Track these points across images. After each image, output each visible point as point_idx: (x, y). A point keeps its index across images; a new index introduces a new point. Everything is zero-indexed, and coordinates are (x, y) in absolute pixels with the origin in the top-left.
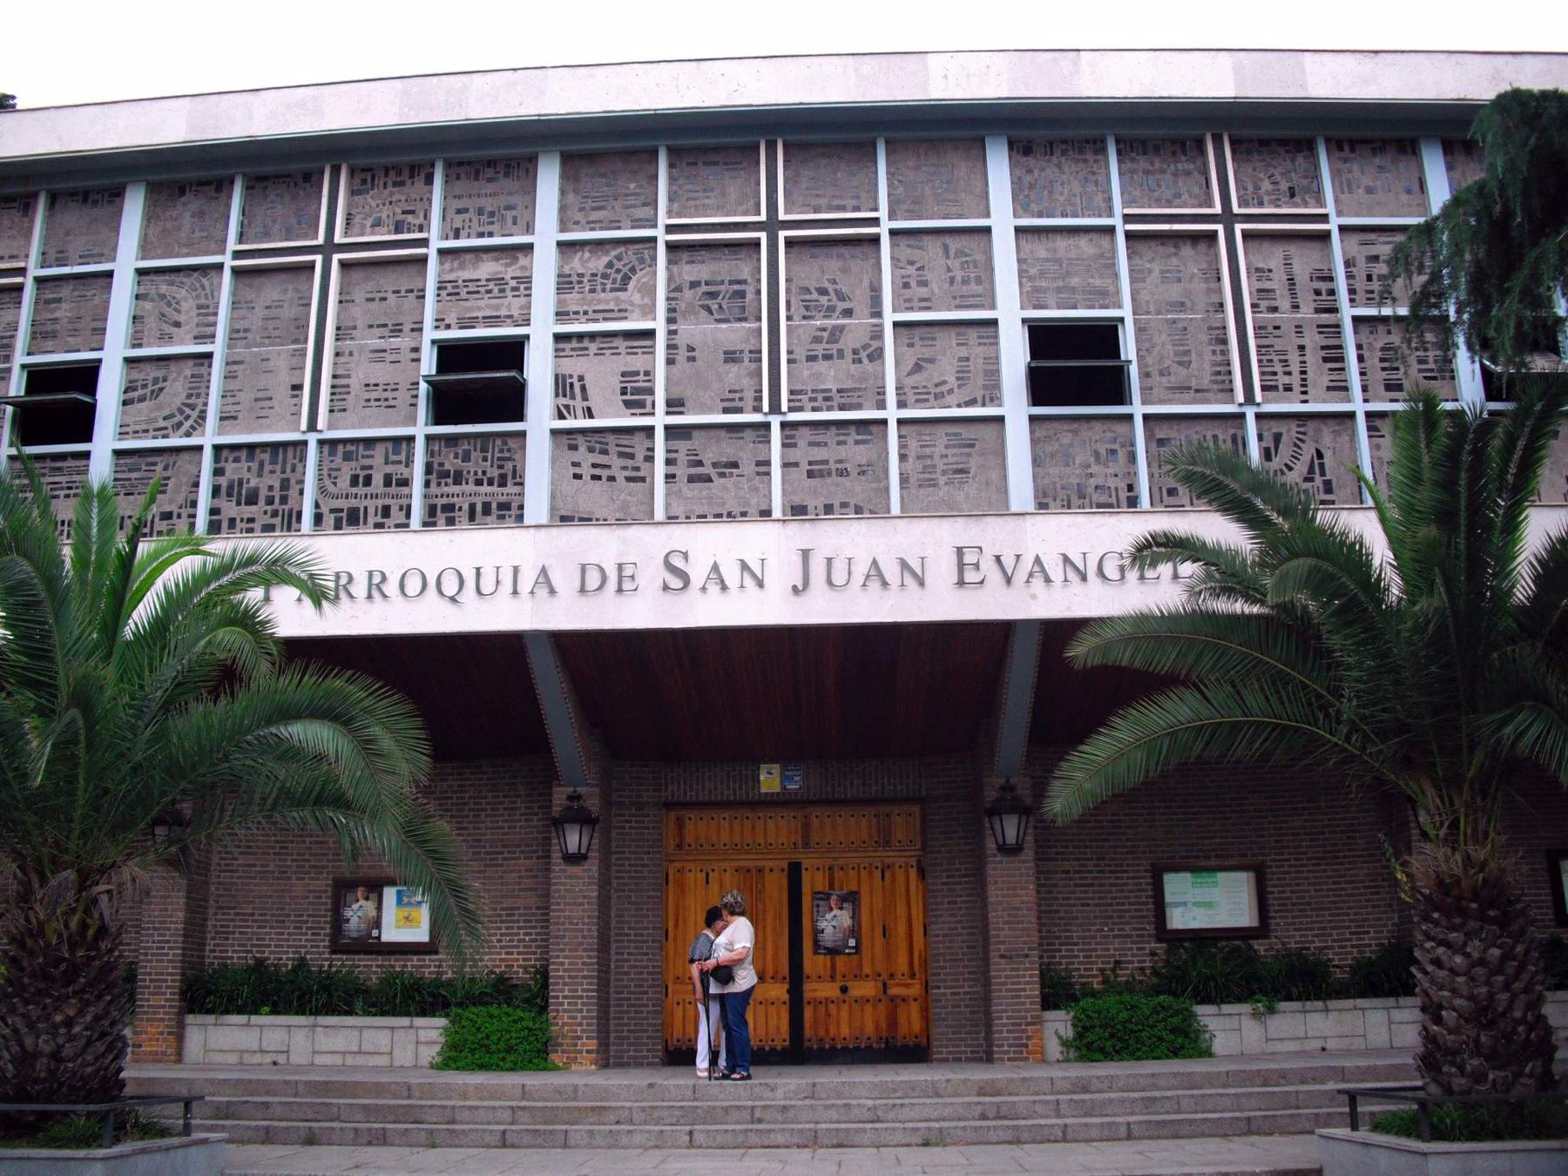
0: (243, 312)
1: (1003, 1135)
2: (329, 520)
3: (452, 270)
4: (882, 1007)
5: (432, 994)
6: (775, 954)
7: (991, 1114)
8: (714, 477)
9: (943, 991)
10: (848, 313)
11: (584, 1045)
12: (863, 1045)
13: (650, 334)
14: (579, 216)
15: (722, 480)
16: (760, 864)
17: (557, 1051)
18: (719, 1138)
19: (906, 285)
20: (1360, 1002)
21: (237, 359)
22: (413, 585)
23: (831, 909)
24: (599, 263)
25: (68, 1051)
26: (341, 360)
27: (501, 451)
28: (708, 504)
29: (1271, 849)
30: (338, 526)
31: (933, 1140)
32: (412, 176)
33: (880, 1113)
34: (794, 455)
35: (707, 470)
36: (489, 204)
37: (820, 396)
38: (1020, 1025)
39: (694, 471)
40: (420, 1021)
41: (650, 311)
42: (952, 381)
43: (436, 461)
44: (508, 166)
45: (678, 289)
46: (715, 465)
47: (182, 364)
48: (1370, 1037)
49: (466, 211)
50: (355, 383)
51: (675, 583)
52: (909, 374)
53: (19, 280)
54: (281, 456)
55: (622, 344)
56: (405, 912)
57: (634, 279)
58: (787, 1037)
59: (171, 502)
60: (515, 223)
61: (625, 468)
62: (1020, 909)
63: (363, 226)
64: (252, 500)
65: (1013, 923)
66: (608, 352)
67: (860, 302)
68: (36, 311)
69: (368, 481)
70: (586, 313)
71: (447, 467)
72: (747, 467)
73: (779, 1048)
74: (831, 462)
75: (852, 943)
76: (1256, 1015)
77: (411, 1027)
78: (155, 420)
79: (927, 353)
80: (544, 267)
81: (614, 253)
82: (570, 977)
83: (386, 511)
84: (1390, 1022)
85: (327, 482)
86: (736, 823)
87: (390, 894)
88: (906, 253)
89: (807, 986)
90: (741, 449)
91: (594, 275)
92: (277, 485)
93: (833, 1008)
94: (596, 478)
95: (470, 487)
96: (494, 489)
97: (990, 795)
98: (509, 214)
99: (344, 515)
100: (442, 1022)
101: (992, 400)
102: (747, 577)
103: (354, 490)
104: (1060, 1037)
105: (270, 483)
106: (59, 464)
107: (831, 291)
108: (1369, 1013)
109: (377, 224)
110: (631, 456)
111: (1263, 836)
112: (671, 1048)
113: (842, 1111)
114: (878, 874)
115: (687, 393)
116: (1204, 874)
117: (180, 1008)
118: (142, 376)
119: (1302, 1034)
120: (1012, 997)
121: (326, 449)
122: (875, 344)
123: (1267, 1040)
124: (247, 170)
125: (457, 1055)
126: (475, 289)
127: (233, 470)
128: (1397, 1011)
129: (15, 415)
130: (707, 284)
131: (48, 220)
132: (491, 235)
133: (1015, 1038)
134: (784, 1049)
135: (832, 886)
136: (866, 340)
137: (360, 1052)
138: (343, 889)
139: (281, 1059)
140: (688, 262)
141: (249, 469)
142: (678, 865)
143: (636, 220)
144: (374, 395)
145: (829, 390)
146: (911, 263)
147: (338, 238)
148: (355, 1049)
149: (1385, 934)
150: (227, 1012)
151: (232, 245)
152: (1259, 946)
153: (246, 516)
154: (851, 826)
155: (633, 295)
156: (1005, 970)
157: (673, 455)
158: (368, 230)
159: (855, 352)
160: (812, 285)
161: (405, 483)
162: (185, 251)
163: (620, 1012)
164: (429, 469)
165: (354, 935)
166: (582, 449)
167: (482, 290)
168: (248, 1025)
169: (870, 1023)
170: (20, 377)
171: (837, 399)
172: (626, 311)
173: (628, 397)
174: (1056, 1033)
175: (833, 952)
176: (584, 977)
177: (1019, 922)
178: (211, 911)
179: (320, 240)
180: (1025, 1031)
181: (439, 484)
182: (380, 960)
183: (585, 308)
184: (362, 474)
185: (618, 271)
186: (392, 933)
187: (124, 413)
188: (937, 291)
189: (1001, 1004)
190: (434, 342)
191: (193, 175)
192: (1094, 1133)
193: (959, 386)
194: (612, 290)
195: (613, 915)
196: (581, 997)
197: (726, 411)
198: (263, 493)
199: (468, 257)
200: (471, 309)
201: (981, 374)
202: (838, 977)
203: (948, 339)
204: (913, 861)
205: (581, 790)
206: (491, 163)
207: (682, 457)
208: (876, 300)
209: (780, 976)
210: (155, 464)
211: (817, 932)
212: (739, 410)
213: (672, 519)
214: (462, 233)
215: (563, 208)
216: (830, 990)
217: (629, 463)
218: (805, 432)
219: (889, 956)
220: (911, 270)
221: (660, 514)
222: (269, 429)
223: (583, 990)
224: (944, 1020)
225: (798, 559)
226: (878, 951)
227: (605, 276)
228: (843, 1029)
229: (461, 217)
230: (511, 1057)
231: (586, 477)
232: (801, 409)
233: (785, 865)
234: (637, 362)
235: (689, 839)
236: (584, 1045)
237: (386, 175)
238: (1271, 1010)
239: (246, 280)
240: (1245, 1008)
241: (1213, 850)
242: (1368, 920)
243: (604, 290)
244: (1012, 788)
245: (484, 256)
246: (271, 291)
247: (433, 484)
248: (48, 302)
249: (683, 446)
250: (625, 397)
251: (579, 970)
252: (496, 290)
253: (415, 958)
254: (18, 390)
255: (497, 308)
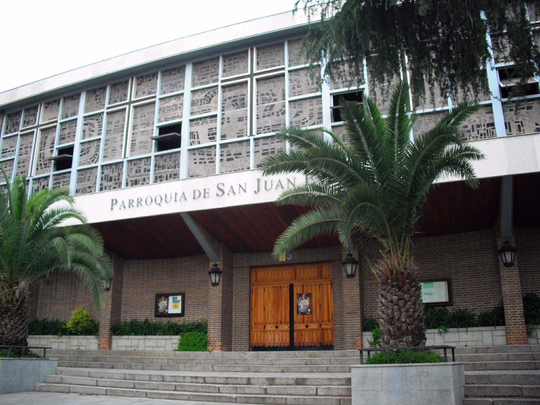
0: (109, 125)
1: (307, 370)
2: (130, 184)
3: (163, 104)
4: (319, 332)
5: (177, 329)
6: (285, 316)
7: (309, 363)
8: (234, 158)
9: (337, 326)
10: (275, 100)
11: (217, 344)
12: (313, 345)
13: (215, 116)
14: (198, 82)
15: (237, 159)
16: (281, 285)
17: (209, 346)
18: (221, 369)
19: (294, 88)
20: (480, 328)
21: (108, 139)
22: (149, 201)
23: (303, 299)
24: (202, 96)
25: (5, 332)
26: (134, 135)
27: (175, 158)
28: (233, 167)
29: (454, 273)
30: (132, 185)
31: (284, 371)
32: (153, 77)
33: (273, 362)
34: (258, 148)
35: (232, 156)
36: (173, 82)
37: (266, 128)
38: (353, 336)
39: (228, 157)
40: (173, 337)
41: (216, 108)
42: (308, 118)
43: (157, 163)
44: (179, 70)
45: (225, 100)
46: (235, 155)
47: (94, 142)
48: (485, 341)
49: (167, 85)
50: (137, 142)
51: (220, 193)
52: (294, 117)
53: (55, 124)
54: (118, 167)
55: (208, 120)
56: (175, 304)
57: (213, 99)
58: (289, 343)
59: (91, 183)
60: (180, 87)
61: (208, 159)
62: (354, 296)
63: (140, 95)
64: (111, 180)
65: (351, 301)
66: (204, 123)
67: (279, 97)
68: (61, 132)
69: (140, 171)
70: (199, 112)
71: (161, 164)
72: (244, 154)
73: (286, 346)
74: (269, 150)
75: (309, 310)
76: (440, 333)
77: (171, 339)
78: (87, 160)
79: (300, 110)
80: (187, 99)
81: (207, 92)
82: (214, 322)
83: (144, 180)
84: (493, 336)
85: (129, 173)
86: (280, 272)
87: (171, 298)
88: (294, 77)
89: (295, 325)
90: (242, 149)
91: (201, 100)
92: (117, 175)
93: (303, 332)
94: (200, 163)
95: (166, 170)
96: (173, 170)
97: (344, 258)
98: (179, 84)
99: (133, 182)
100: (178, 337)
101: (320, 123)
102: (241, 189)
103: (136, 174)
104: (369, 341)
105: (115, 175)
106: (65, 175)
107: (271, 94)
108: (484, 332)
109: (144, 93)
110: (210, 155)
111: (451, 268)
112: (253, 346)
113: (262, 361)
114: (318, 287)
115: (227, 133)
116: (429, 283)
117: (110, 334)
118: (84, 147)
119: (458, 340)
120: (351, 327)
121: (129, 163)
122: (283, 109)
123: (444, 342)
124: (110, 83)
125: (184, 346)
126: (169, 109)
127: (107, 172)
128: (495, 331)
129: (54, 162)
130: (234, 97)
131: (64, 105)
132: (174, 91)
133: (352, 341)
134: (288, 346)
135: (303, 292)
136: (281, 108)
137: (157, 347)
138: (159, 297)
139: (136, 349)
140: (228, 91)
141: (110, 171)
142: (256, 286)
143: (215, 80)
144: (142, 145)
145: (269, 126)
146: (295, 80)
147: (255, 71)
148: (156, 345)
149: (497, 303)
150: (123, 335)
151: (107, 105)
152: (449, 309)
153: (109, 185)
154: (311, 272)
155: (212, 104)
156: (348, 318)
157: (223, 153)
158: (141, 95)
159: (277, 112)
160: (265, 92)
161: (149, 171)
162: (95, 109)
163: (236, 334)
164: (156, 166)
165: (161, 312)
166: (197, 154)
167: (171, 109)
168: (128, 339)
169: (315, 338)
170: (56, 152)
171: (272, 129)
172: (210, 109)
173: (210, 136)
174: (368, 340)
175: (302, 313)
176: (218, 322)
177: (354, 301)
178: (122, 305)
179: (249, 73)
180: (356, 339)
181: (158, 170)
182: (168, 319)
183: (199, 110)
184: (138, 169)
185: (208, 97)
186: (171, 311)
187: (80, 159)
188: (303, 88)
189: (347, 330)
190: (157, 127)
191: (97, 87)
192: (337, 369)
193: (310, 119)
194: (207, 103)
195: (233, 303)
196: (217, 329)
197: (238, 137)
198: (114, 178)
199: (168, 99)
200: (168, 115)
201: (317, 114)
202: (305, 322)
203: (307, 104)
204: (329, 283)
205: (217, 263)
206: (174, 69)
207: (225, 154)
208: (284, 95)
209: (287, 322)
210: (87, 173)
211: (298, 307)
212: (242, 136)
213: (222, 173)
214: (166, 92)
215: (193, 80)
216: (302, 327)
217: (210, 157)
218: (261, 141)
219: (322, 314)
220: (296, 83)
221: (217, 172)
222: (115, 158)
223: (217, 326)
224: (338, 336)
225: (256, 182)
226: (318, 314)
227: (204, 99)
228: (307, 340)
229: (166, 87)
230: (195, 348)
231: (198, 163)
232: (260, 133)
233: (288, 285)
234: (212, 125)
235: (259, 277)
236: (217, 344)
237: (146, 78)
238: (446, 331)
239: (110, 115)
240: (436, 331)
241: (432, 274)
242: (490, 298)
243: (204, 104)
244: (351, 255)
245: (171, 98)
246: (117, 117)
247: (157, 170)
248: (63, 129)
249: (225, 150)
250: (209, 137)
251: (216, 320)
252: (174, 108)
253: (178, 318)
254: (56, 154)
255: (175, 114)
